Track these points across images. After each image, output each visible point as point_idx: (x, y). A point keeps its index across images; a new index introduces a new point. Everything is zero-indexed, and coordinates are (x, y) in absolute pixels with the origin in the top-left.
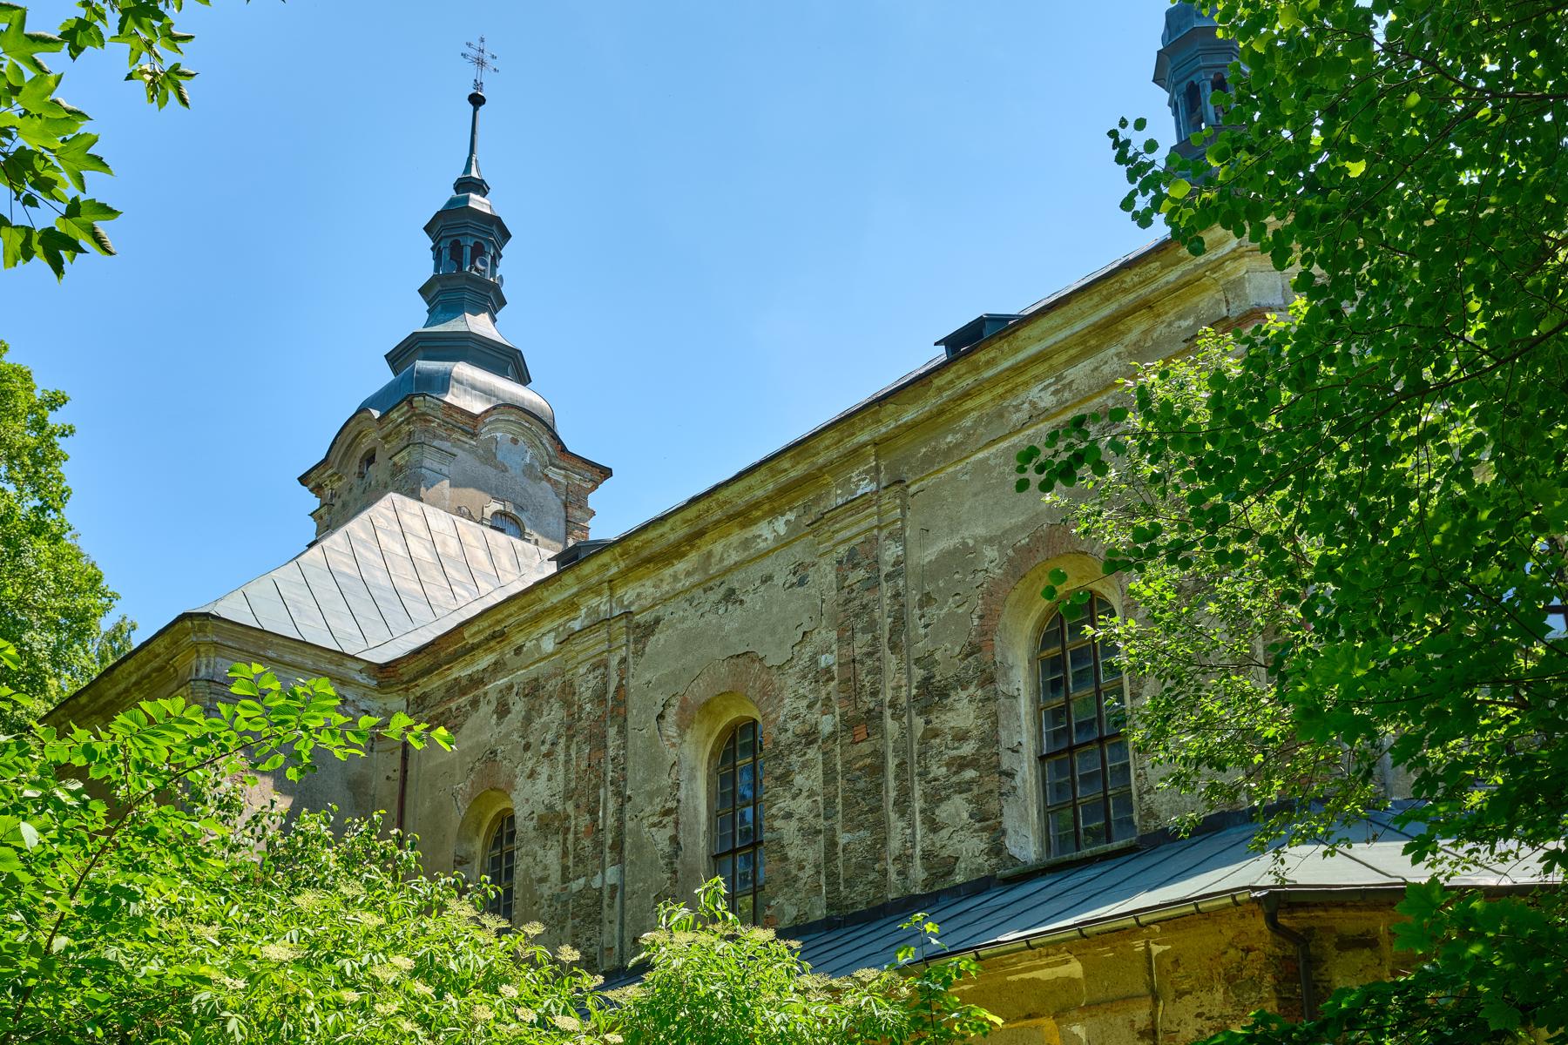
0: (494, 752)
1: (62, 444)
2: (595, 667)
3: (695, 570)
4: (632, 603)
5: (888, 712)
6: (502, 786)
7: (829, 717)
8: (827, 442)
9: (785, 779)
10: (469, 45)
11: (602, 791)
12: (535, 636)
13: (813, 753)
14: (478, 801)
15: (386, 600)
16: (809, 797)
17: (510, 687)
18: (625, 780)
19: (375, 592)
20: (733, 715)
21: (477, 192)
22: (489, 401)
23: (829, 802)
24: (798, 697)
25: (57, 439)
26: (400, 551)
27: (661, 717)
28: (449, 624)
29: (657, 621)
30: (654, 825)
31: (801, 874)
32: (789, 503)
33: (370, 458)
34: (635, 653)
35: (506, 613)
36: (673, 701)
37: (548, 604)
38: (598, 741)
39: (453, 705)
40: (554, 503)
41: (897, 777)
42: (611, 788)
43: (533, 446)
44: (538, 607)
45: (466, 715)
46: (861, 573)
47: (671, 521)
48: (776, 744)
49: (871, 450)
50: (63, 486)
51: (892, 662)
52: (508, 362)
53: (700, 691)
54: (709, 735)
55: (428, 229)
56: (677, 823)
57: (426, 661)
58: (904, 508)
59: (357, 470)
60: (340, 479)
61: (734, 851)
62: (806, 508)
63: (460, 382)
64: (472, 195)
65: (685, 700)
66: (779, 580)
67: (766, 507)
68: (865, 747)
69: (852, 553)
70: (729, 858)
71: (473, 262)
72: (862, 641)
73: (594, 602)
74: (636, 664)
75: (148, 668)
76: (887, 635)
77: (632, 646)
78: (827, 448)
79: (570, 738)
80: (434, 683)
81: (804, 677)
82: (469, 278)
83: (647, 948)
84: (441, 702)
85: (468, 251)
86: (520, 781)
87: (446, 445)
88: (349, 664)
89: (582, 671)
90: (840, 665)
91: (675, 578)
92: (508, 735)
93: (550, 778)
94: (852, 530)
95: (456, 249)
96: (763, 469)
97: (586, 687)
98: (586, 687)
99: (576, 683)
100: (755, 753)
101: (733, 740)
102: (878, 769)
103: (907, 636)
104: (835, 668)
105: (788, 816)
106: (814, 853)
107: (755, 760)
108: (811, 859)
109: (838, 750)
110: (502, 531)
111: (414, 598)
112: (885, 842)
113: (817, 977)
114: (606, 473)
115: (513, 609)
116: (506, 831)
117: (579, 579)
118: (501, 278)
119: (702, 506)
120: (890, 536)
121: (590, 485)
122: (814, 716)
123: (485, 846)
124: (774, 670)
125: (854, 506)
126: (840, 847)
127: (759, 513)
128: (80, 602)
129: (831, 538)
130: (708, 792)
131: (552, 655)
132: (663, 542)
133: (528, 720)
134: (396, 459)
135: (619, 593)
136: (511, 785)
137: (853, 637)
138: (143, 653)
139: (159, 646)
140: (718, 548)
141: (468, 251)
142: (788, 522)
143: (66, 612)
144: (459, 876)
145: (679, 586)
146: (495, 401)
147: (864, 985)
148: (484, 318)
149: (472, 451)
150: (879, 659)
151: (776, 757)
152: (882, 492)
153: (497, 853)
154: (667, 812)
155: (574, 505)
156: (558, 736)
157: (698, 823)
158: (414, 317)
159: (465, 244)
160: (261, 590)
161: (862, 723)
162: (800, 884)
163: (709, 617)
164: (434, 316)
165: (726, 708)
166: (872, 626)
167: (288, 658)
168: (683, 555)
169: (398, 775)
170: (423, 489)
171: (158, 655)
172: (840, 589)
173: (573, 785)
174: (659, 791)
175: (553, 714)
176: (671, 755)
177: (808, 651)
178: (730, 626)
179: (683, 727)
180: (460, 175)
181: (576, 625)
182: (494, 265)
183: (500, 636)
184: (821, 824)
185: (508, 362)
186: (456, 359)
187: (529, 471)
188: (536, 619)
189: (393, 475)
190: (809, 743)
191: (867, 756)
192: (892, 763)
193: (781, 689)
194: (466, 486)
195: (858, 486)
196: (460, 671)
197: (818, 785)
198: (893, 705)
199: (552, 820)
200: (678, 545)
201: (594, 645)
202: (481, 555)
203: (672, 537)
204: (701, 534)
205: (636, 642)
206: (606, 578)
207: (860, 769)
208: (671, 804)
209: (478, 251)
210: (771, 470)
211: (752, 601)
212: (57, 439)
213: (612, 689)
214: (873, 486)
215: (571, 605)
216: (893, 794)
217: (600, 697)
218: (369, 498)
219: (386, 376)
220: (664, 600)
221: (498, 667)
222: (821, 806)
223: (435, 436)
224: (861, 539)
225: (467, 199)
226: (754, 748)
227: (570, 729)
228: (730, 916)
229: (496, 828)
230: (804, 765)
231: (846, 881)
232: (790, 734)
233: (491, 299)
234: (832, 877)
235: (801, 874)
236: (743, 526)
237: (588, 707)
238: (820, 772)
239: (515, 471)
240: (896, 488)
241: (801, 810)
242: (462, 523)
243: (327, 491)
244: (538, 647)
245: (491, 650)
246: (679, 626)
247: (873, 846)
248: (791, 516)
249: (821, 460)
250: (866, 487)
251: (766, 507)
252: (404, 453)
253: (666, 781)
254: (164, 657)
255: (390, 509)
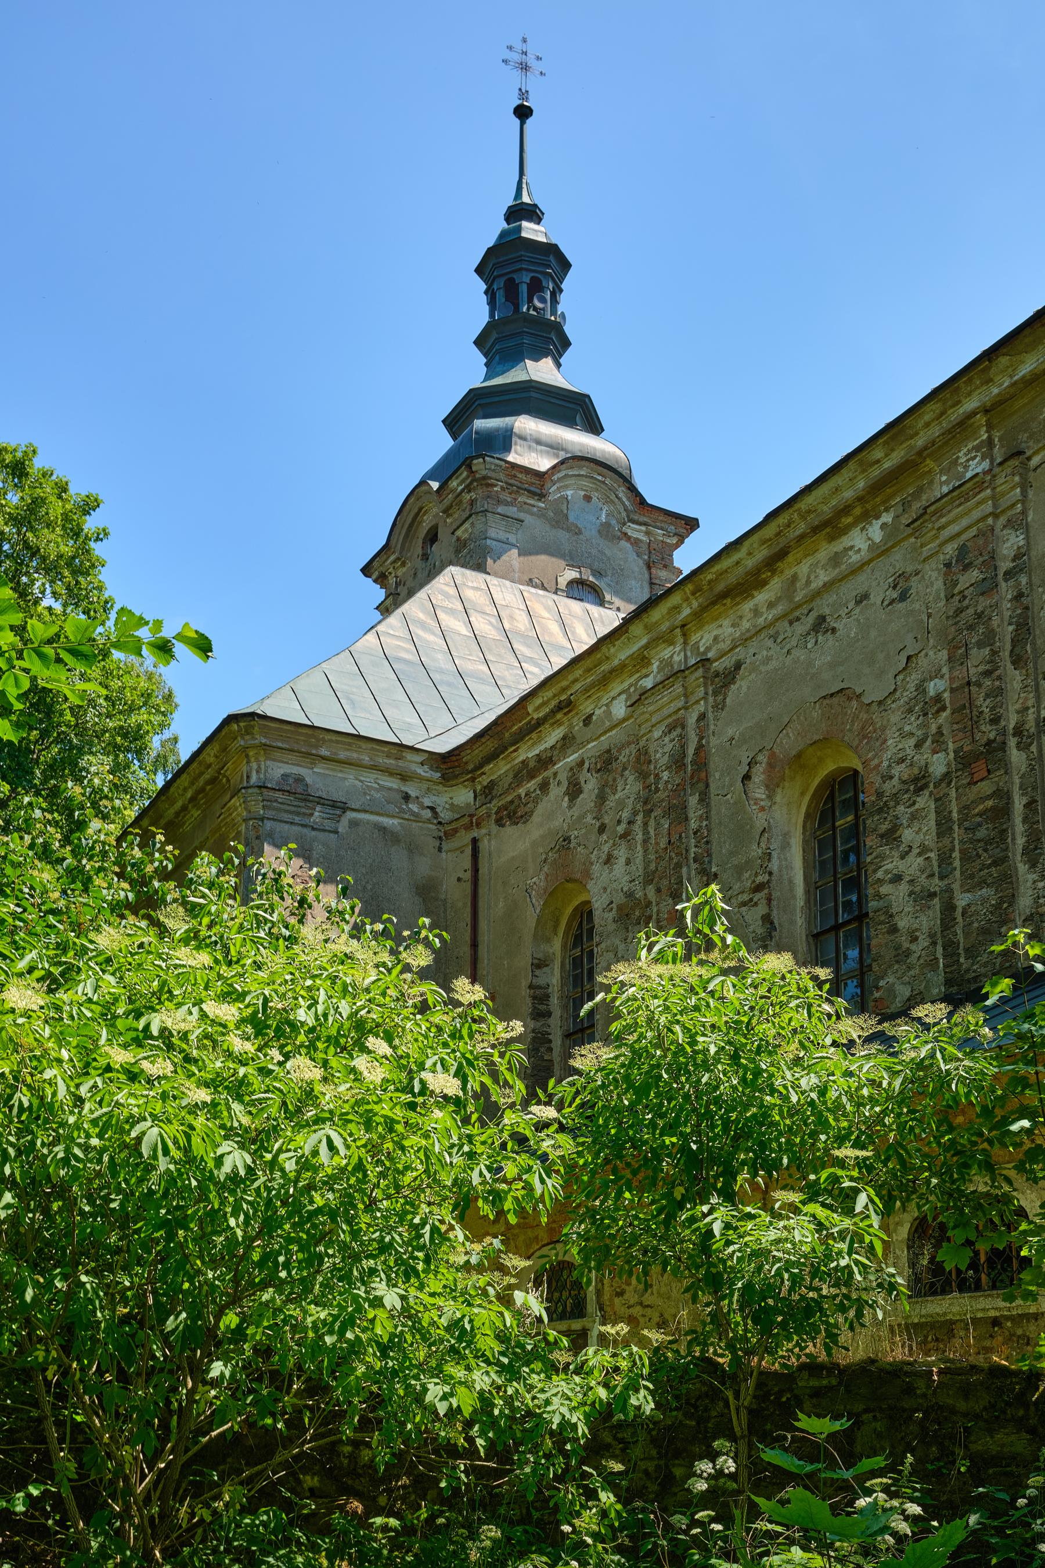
0: (567, 839)
1: (98, 549)
2: (671, 729)
3: (779, 599)
4: (708, 649)
5: (1012, 742)
6: (578, 876)
7: (941, 755)
8: (927, 418)
9: (891, 836)
10: (510, 48)
11: (684, 870)
12: (604, 701)
13: (923, 801)
14: (553, 895)
15: (449, 684)
16: (920, 854)
17: (581, 763)
18: (709, 855)
19: (436, 677)
20: (830, 767)
21: (530, 220)
22: (558, 456)
23: (945, 859)
24: (904, 736)
25: (92, 544)
26: (465, 631)
27: (747, 777)
28: (513, 697)
29: (738, 666)
30: (744, 904)
31: (913, 947)
32: (883, 502)
33: (432, 537)
34: (715, 707)
35: (571, 678)
36: (760, 758)
37: (616, 662)
38: (678, 813)
39: (522, 791)
40: (635, 564)
41: (1025, 820)
42: (694, 866)
43: (608, 501)
44: (605, 667)
45: (536, 801)
46: (975, 575)
47: (747, 544)
48: (880, 794)
49: (981, 419)
50: (106, 596)
51: (1015, 678)
52: (575, 409)
53: (789, 743)
54: (803, 794)
55: (479, 271)
56: (769, 900)
57: (491, 745)
58: (1025, 486)
59: (420, 551)
60: (403, 564)
61: (837, 927)
62: (906, 505)
63: (523, 438)
64: (525, 224)
65: (773, 755)
66: (876, 598)
67: (858, 511)
68: (986, 787)
69: (963, 550)
70: (831, 936)
71: (530, 300)
72: (979, 655)
73: (666, 652)
74: (716, 719)
75: (201, 782)
76: (1008, 646)
77: (711, 699)
78: (927, 425)
79: (648, 813)
80: (500, 770)
81: (910, 711)
82: (527, 318)
83: (607, 989)
84: (510, 788)
85: (524, 289)
86: (596, 868)
87: (512, 511)
88: (409, 756)
89: (657, 734)
90: (953, 690)
91: (756, 612)
92: (582, 817)
93: (628, 862)
94: (960, 523)
95: (511, 291)
96: (852, 465)
97: (661, 753)
98: (661, 753)
99: (651, 750)
100: (857, 810)
101: (831, 797)
102: (1001, 813)
103: (1033, 644)
104: (946, 695)
105: (897, 879)
106: (929, 920)
107: (857, 817)
108: (925, 928)
109: (953, 794)
110: (581, 600)
111: (481, 680)
112: (1012, 899)
113: (860, 1021)
114: (692, 524)
115: (578, 672)
116: (585, 927)
117: (648, 628)
118: (563, 315)
119: (782, 520)
120: (1010, 524)
121: (674, 540)
122: (925, 756)
123: (564, 946)
124: (874, 706)
125: (963, 492)
126: (959, 910)
127: (849, 520)
128: (133, 720)
129: (936, 537)
130: (805, 860)
131: (624, 720)
132: (740, 570)
133: (602, 798)
134: (459, 533)
135: (694, 638)
136: (587, 874)
137: (966, 655)
138: (195, 765)
139: (209, 756)
140: (803, 569)
141: (524, 289)
142: (884, 526)
143: (123, 732)
144: (389, 920)
145: (761, 621)
146: (563, 455)
147: (927, 1027)
148: (547, 363)
149: (542, 515)
150: (999, 678)
151: (880, 811)
152: (996, 470)
153: (577, 952)
154: (758, 888)
155: (658, 557)
156: (635, 813)
157: (794, 897)
158: (472, 372)
159: (521, 280)
160: (311, 684)
161: (982, 758)
162: (912, 960)
163: (796, 653)
164: (492, 368)
165: (821, 760)
166: (989, 639)
167: (343, 755)
168: (764, 583)
169: (468, 875)
170: (489, 561)
171: (209, 766)
172: (949, 597)
173: (653, 866)
174: (748, 864)
175: (629, 788)
176: (760, 821)
177: (914, 678)
178: (821, 660)
179: (771, 787)
180: (511, 203)
181: (648, 683)
182: (555, 301)
183: (566, 706)
184: (936, 885)
185: (575, 409)
186: (516, 413)
187: (605, 530)
188: (604, 681)
189: (458, 551)
190: (918, 790)
191: (989, 797)
192: (1019, 803)
193: (883, 729)
194: (537, 553)
195: (966, 467)
196: (527, 752)
197: (930, 840)
198: (1018, 732)
199: (633, 909)
200: (757, 571)
201: (668, 702)
202: (555, 628)
203: (750, 563)
204: (782, 555)
205: (715, 693)
206: (678, 623)
207: (980, 815)
208: (762, 878)
209: (536, 287)
210: (861, 463)
211: (848, 628)
212: (92, 544)
213: (691, 751)
214: (986, 465)
215: (641, 660)
216: (1021, 841)
217: (678, 762)
218: (432, 574)
219: (445, 442)
220: (745, 640)
221: (567, 743)
222: (935, 864)
223: (499, 502)
224: (973, 532)
225: (519, 229)
226: (854, 805)
227: (647, 804)
228: (730, 939)
229: (575, 924)
230: (913, 817)
231: (966, 950)
232: (895, 781)
233: (553, 340)
234: (950, 947)
235: (913, 947)
236: (832, 538)
237: (665, 776)
238: (933, 823)
239: (590, 532)
240: (1014, 462)
241: (911, 871)
242: (529, 591)
243: (392, 580)
244: (608, 713)
245: (559, 723)
246: (763, 668)
247: (998, 906)
248: (887, 518)
249: (920, 442)
250: (977, 466)
251: (858, 511)
252: (467, 525)
253: (755, 851)
254: (215, 767)
255: (452, 583)
